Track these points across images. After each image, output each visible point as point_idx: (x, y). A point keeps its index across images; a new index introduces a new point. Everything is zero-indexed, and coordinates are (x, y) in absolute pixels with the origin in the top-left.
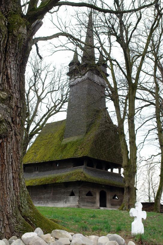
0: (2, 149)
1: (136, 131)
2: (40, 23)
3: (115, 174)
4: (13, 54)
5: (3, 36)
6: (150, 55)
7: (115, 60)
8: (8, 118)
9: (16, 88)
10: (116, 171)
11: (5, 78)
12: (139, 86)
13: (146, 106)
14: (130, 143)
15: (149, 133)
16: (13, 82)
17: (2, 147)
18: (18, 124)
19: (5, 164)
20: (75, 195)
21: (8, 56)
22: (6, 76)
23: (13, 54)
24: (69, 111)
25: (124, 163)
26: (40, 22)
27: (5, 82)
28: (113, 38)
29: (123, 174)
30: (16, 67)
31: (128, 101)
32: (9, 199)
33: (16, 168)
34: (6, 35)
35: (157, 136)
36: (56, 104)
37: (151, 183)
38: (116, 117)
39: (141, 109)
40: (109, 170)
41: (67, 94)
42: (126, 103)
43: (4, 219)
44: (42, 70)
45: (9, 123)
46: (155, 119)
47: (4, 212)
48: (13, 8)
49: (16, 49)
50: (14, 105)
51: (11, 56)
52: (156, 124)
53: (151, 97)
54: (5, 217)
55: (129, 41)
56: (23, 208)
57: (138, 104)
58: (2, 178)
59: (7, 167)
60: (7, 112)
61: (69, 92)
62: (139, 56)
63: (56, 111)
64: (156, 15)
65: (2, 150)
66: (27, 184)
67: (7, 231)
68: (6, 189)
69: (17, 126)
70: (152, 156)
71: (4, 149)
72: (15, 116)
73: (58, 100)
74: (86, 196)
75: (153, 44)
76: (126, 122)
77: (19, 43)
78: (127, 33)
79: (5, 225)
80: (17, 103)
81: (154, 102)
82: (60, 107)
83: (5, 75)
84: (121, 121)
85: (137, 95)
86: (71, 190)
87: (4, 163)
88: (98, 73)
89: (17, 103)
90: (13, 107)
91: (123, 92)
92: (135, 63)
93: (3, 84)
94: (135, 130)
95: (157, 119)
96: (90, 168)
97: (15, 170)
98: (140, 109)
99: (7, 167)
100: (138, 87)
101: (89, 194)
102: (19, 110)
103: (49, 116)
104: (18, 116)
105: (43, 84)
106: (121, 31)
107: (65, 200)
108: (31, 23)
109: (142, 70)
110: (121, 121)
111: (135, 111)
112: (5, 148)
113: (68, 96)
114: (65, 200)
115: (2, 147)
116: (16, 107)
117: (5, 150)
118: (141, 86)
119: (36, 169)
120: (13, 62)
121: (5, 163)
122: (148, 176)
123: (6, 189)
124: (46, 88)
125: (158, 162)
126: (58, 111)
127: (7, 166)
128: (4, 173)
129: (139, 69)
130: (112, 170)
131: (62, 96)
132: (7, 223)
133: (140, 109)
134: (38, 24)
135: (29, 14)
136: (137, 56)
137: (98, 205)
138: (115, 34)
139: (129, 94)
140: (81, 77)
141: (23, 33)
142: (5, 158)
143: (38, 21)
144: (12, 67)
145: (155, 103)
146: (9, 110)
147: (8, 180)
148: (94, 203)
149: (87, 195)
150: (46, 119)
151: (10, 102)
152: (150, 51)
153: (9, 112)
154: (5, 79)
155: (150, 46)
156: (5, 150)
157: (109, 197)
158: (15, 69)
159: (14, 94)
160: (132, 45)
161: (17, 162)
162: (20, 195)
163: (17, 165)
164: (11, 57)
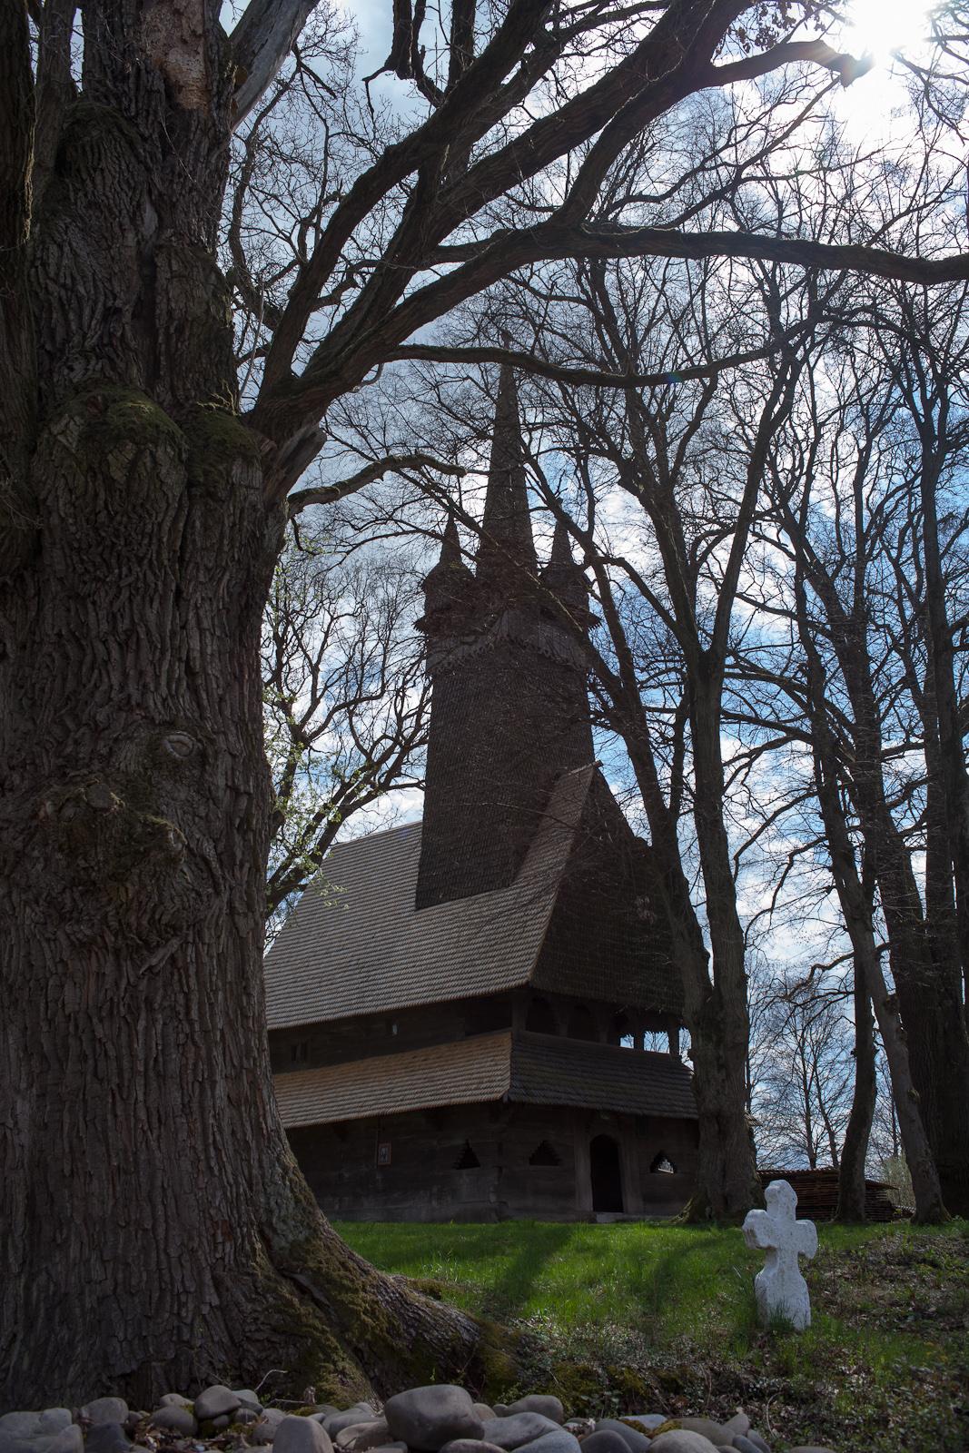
0: (180, 975)
1: (736, 858)
2: (317, 439)
3: (656, 1056)
4: (208, 569)
5: (168, 505)
6: (771, 531)
7: (621, 562)
8: (198, 840)
9: (227, 712)
10: (657, 1042)
11: (183, 674)
12: (730, 660)
13: (771, 746)
14: (710, 913)
15: (791, 865)
16: (215, 686)
17: (179, 970)
18: (242, 866)
19: (194, 1043)
20: (478, 1165)
21: (190, 581)
22: (183, 665)
23: (208, 569)
24: (432, 787)
25: (693, 1000)
26: (314, 435)
27: (182, 691)
28: (603, 469)
29: (691, 1055)
30: (222, 626)
31: (687, 728)
32: (219, 1194)
33: (241, 1058)
34: (180, 499)
35: (827, 877)
36: (376, 756)
37: (814, 1089)
38: (639, 803)
39: (749, 765)
40: (627, 1043)
41: (420, 711)
42: (678, 741)
43: (201, 1285)
44: (308, 615)
45: (207, 862)
46: (814, 802)
47: (200, 1253)
48: (203, 387)
49: (220, 549)
50: (221, 782)
51: (202, 579)
52: (819, 827)
53: (788, 707)
54: (207, 1277)
55: (672, 479)
56: (275, 1231)
57: (729, 745)
58: (183, 1104)
59: (203, 1052)
60: (195, 815)
61: (428, 701)
62: (720, 535)
63: (373, 785)
64: (778, 367)
65: (180, 980)
66: (286, 1123)
67: (216, 1339)
68: (206, 1150)
69: (238, 874)
70: (813, 969)
71: (188, 976)
72: (224, 833)
73: (385, 737)
74: (531, 1164)
75: (776, 480)
76: (686, 827)
77: (234, 524)
78: (662, 446)
79: (205, 1310)
80: (233, 774)
81: (806, 726)
82: (395, 771)
83: (180, 659)
84: (663, 821)
85: (727, 702)
86: (459, 1142)
87: (190, 1036)
88: (548, 615)
89: (233, 774)
90: (220, 794)
91: (661, 698)
92: (705, 565)
93: (172, 697)
94: (731, 857)
95: (822, 800)
96: (539, 1034)
97: (234, 1066)
98: (746, 760)
99: (203, 1052)
100: (729, 667)
101: (544, 1155)
102: (244, 802)
103: (346, 811)
104: (238, 829)
105: (315, 670)
106: (640, 446)
107: (435, 1189)
108: (278, 442)
109: (741, 596)
110: (663, 821)
111: (723, 774)
112: (192, 970)
113: (425, 718)
114: (435, 1189)
115: (179, 970)
116: (228, 791)
117: (193, 981)
118: (742, 659)
119: (298, 1054)
120: (211, 605)
121: (193, 1039)
122: (798, 1059)
123: (206, 1150)
124: (326, 688)
125: (840, 992)
126: (385, 787)
127: (203, 1047)
128: (193, 1083)
129: (728, 590)
130: (639, 1042)
131: (400, 719)
132: (216, 1301)
133: (746, 760)
134: (303, 443)
135: (265, 405)
136: (711, 533)
137: (587, 1202)
138: (614, 454)
139: (688, 699)
140: (475, 641)
141: (247, 483)
142: (194, 1015)
143: (306, 432)
144: (206, 624)
145: (810, 732)
146: (202, 808)
147: (212, 1112)
148: (569, 1194)
149: (533, 1161)
150: (333, 828)
151: (203, 771)
152: (768, 513)
153: (201, 818)
154: (179, 679)
155: (766, 492)
156: (193, 981)
157: (631, 1164)
158: (218, 633)
159: (221, 738)
160: (693, 501)
161: (241, 1030)
162: (263, 1176)
163: (242, 1043)
164: (201, 583)
